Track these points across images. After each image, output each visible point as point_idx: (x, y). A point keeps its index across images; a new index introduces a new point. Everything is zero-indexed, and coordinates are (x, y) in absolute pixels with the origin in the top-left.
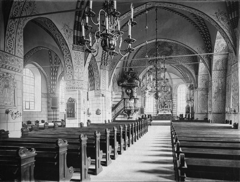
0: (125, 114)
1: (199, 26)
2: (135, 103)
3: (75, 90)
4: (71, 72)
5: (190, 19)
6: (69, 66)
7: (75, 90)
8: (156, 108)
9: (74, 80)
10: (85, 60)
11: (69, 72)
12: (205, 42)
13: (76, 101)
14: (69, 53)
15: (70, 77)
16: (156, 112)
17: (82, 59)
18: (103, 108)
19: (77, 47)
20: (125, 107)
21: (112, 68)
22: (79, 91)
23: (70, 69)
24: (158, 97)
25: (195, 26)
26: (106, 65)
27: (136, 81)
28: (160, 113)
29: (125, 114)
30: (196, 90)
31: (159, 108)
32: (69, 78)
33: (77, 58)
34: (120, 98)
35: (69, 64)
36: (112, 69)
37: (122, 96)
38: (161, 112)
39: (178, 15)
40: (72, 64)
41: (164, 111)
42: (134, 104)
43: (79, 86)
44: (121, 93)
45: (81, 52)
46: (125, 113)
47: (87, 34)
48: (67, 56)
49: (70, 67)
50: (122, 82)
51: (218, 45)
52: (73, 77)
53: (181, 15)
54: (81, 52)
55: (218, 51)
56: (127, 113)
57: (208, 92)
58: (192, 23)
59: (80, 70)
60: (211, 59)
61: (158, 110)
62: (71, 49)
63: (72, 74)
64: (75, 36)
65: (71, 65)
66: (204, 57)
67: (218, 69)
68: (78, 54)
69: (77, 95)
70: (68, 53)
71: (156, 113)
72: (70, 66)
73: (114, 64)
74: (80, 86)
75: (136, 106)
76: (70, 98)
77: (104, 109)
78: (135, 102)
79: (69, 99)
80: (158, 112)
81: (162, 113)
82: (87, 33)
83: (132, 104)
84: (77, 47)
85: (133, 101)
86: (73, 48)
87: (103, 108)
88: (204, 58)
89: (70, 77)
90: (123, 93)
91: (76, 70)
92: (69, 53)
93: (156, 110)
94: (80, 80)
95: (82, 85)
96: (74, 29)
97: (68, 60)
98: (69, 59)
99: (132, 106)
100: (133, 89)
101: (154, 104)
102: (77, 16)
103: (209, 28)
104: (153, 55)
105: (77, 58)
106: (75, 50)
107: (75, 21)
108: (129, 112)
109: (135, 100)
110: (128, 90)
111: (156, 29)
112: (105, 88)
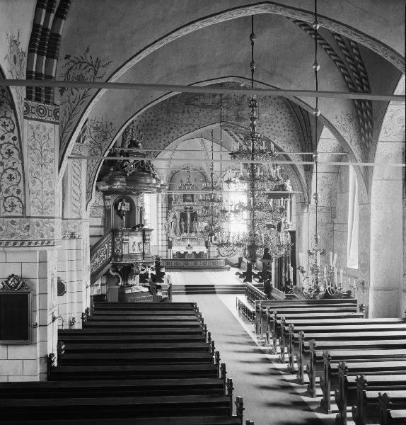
0: (114, 274)
1: (347, 67)
2: (144, 242)
3: (30, 251)
4: (18, 192)
5: (327, 44)
6: (10, 172)
7: (30, 251)
8: (164, 232)
9: (28, 217)
10: (62, 152)
11: (11, 188)
12: (359, 112)
13: (33, 284)
14: (16, 130)
15: (13, 206)
16: (165, 243)
17: (52, 146)
18: (71, 277)
19: (38, 109)
20: (114, 256)
21: (96, 149)
22: (44, 254)
23: (14, 182)
24: (249, 247)
25: (333, 57)
26: (83, 142)
27: (148, 181)
28: (175, 249)
29: (114, 274)
30: (306, 210)
31: (172, 235)
32: (9, 209)
33: (38, 146)
34: (98, 227)
35: (10, 165)
36: (99, 153)
37: (104, 220)
38: (179, 245)
39: (299, 28)
40: (23, 164)
41: (188, 242)
42: (141, 247)
43: (42, 236)
44: (101, 212)
45: (49, 126)
46: (113, 271)
47: (69, 67)
48: (6, 140)
49: (13, 173)
50: (110, 182)
51: (392, 117)
52: (24, 207)
53: (305, 30)
54: (52, 126)
55: (389, 132)
56: (119, 273)
57: (334, 217)
58: (326, 49)
59: (46, 183)
60: (369, 149)
61: (171, 239)
62: (22, 117)
63: (19, 196)
64: (32, 72)
65: (20, 169)
66: (351, 141)
67: (386, 175)
68: (41, 130)
69: (38, 264)
70: (12, 131)
71: (165, 248)
72: (13, 169)
73: (105, 138)
74: (46, 237)
75: (146, 252)
76: (13, 275)
77: (75, 279)
78: (144, 240)
79: (9, 279)
80: (170, 246)
81: (182, 250)
82: (68, 64)
83: (136, 247)
84: (38, 109)
85: (137, 238)
86: (26, 112)
87: (71, 277)
88: (353, 142)
89: (13, 206)
90: (107, 212)
91: (34, 182)
92: (16, 130)
93: (165, 238)
94: (47, 215)
95: (51, 234)
96: (31, 50)
97: (10, 153)
98: (15, 150)
99: (137, 251)
100: (134, 199)
101: (160, 222)
102: (44, 11)
103: (368, 71)
104: (193, 104)
105: (38, 146)
106: (32, 119)
107: (35, 26)
108: (127, 271)
109: (144, 236)
110: (120, 204)
111: (252, 36)
112: (80, 213)
